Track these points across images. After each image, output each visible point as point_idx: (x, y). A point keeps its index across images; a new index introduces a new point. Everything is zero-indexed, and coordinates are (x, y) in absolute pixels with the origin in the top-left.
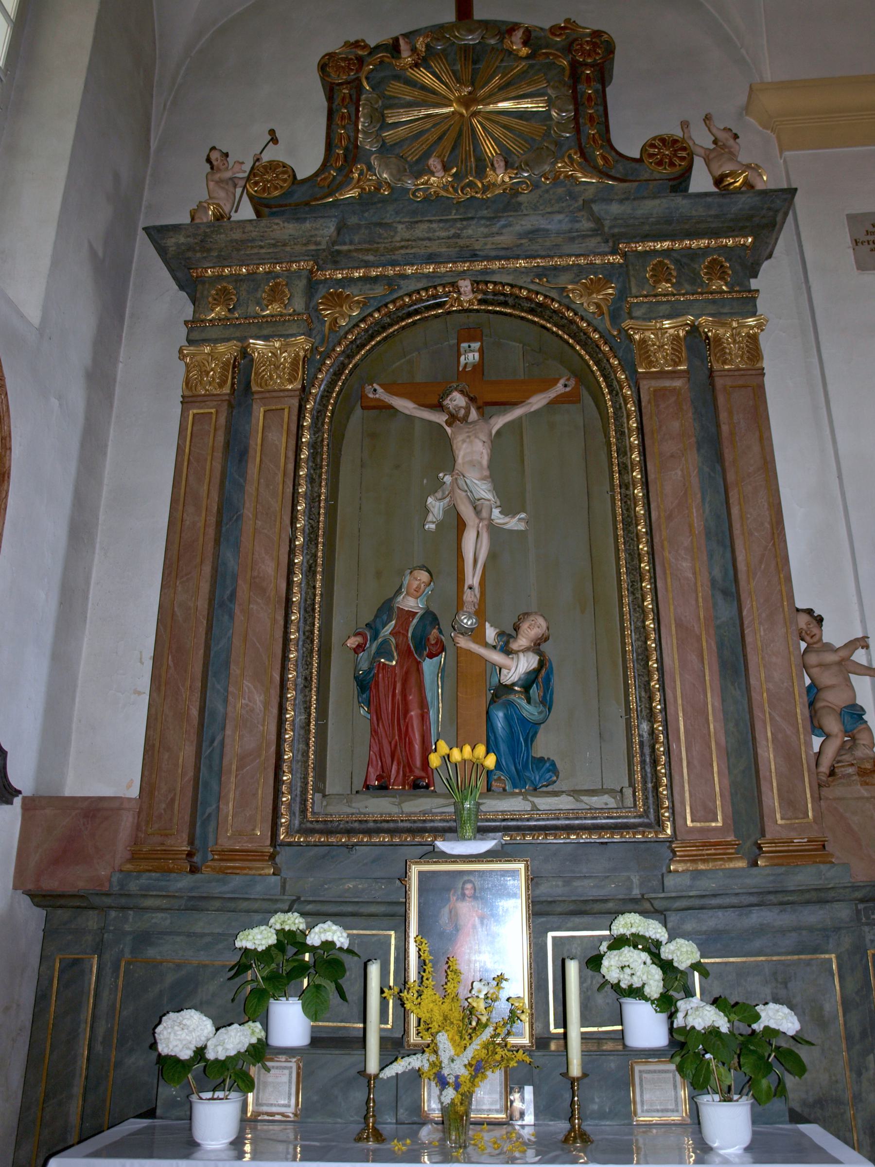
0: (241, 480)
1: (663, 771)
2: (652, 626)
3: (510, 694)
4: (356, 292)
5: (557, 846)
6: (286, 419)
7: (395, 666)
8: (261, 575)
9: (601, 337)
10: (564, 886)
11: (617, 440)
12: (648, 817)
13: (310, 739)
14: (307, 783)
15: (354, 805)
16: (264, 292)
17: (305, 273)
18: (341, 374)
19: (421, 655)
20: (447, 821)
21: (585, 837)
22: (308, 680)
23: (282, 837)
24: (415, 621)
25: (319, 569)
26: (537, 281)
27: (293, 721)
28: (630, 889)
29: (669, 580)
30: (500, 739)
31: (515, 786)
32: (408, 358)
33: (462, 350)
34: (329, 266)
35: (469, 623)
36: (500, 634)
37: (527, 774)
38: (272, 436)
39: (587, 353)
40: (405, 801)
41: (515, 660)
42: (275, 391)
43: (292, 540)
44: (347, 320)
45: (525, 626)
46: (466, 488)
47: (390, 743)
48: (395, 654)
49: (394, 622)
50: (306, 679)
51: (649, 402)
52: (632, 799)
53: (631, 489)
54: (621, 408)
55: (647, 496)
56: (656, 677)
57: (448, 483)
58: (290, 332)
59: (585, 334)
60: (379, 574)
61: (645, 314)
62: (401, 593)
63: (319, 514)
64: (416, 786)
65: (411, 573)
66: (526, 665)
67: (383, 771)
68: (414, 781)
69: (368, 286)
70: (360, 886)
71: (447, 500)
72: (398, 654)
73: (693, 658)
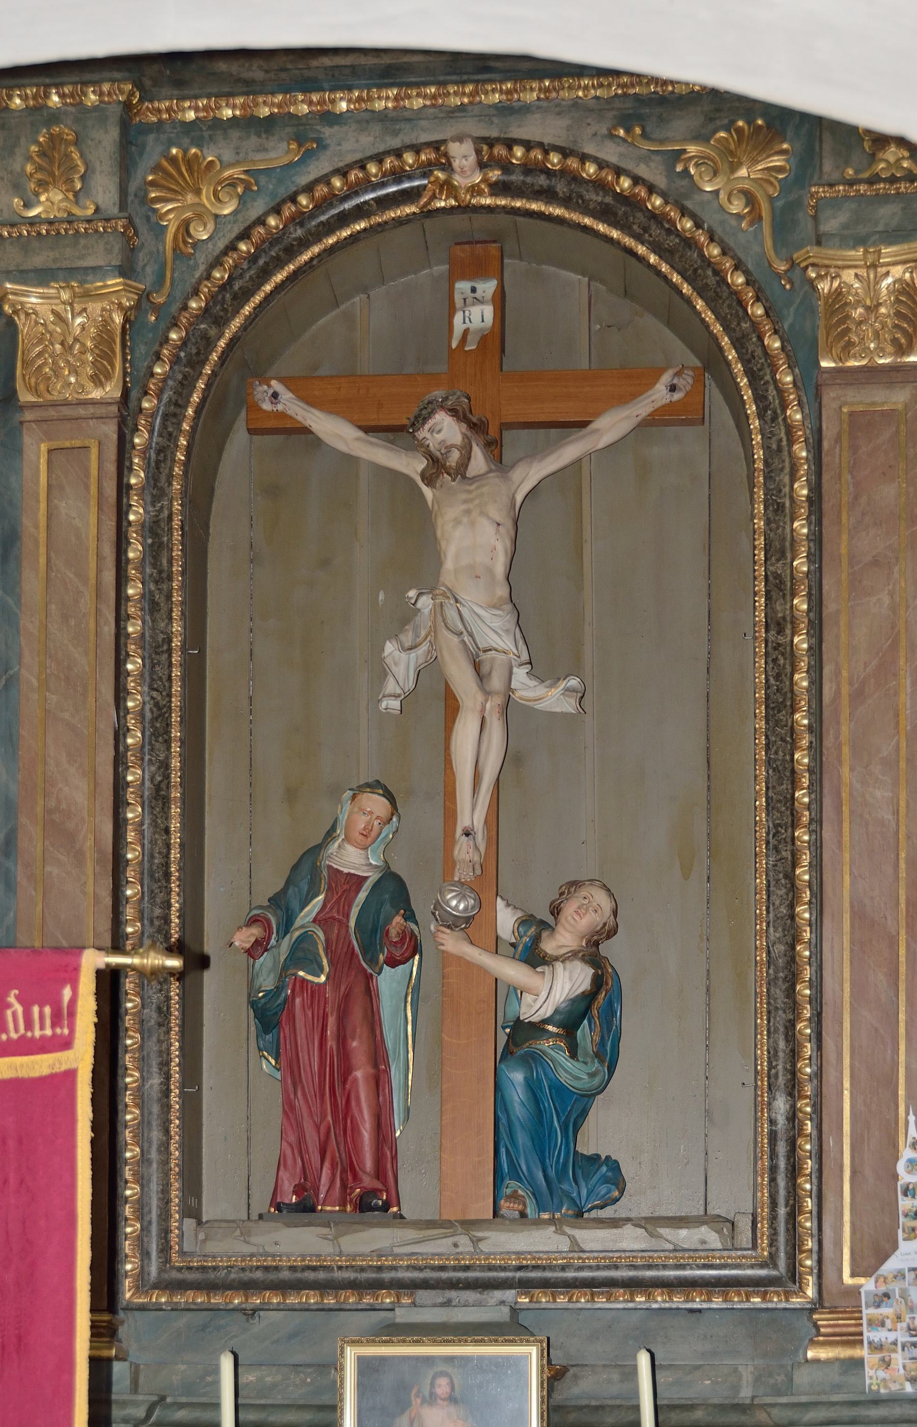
0: (10, 601)
1: (808, 1186)
2: (807, 915)
3: (539, 1038)
4: (228, 155)
5: (613, 1312)
6: (94, 472)
7: (325, 984)
8: (64, 806)
9: (747, 283)
10: (622, 1381)
11: (768, 522)
12: (775, 1266)
13: (170, 1122)
14: (168, 1202)
15: (254, 1239)
16: (29, 158)
17: (115, 112)
18: (203, 363)
19: (373, 961)
20: (420, 1269)
21: (660, 1300)
22: (161, 712)
23: (128, 1295)
24: (362, 896)
25: (176, 794)
26: (622, 132)
27: (139, 1089)
28: (736, 1388)
29: (846, 825)
30: (517, 1124)
31: (541, 1207)
32: (343, 307)
33: (458, 301)
34: (165, 91)
35: (462, 906)
36: (527, 921)
37: (565, 1186)
38: (67, 507)
39: (717, 318)
40: (346, 1234)
41: (548, 976)
42: (66, 403)
43: (120, 733)
44: (211, 226)
45: (569, 909)
46: (461, 627)
47: (318, 1128)
48: (325, 962)
49: (321, 897)
50: (159, 1010)
51: (838, 439)
52: (749, 1234)
53: (788, 632)
54: (780, 450)
55: (816, 651)
56: (807, 1013)
57: (426, 611)
58: (90, 262)
59: (716, 273)
60: (291, 795)
61: (845, 226)
62: (335, 839)
63: (170, 678)
64: (363, 1206)
65: (354, 797)
66: (568, 987)
67: (306, 1179)
68: (361, 1197)
69: (254, 141)
70: (268, 1379)
71: (424, 648)
72: (331, 963)
73: (880, 978)
